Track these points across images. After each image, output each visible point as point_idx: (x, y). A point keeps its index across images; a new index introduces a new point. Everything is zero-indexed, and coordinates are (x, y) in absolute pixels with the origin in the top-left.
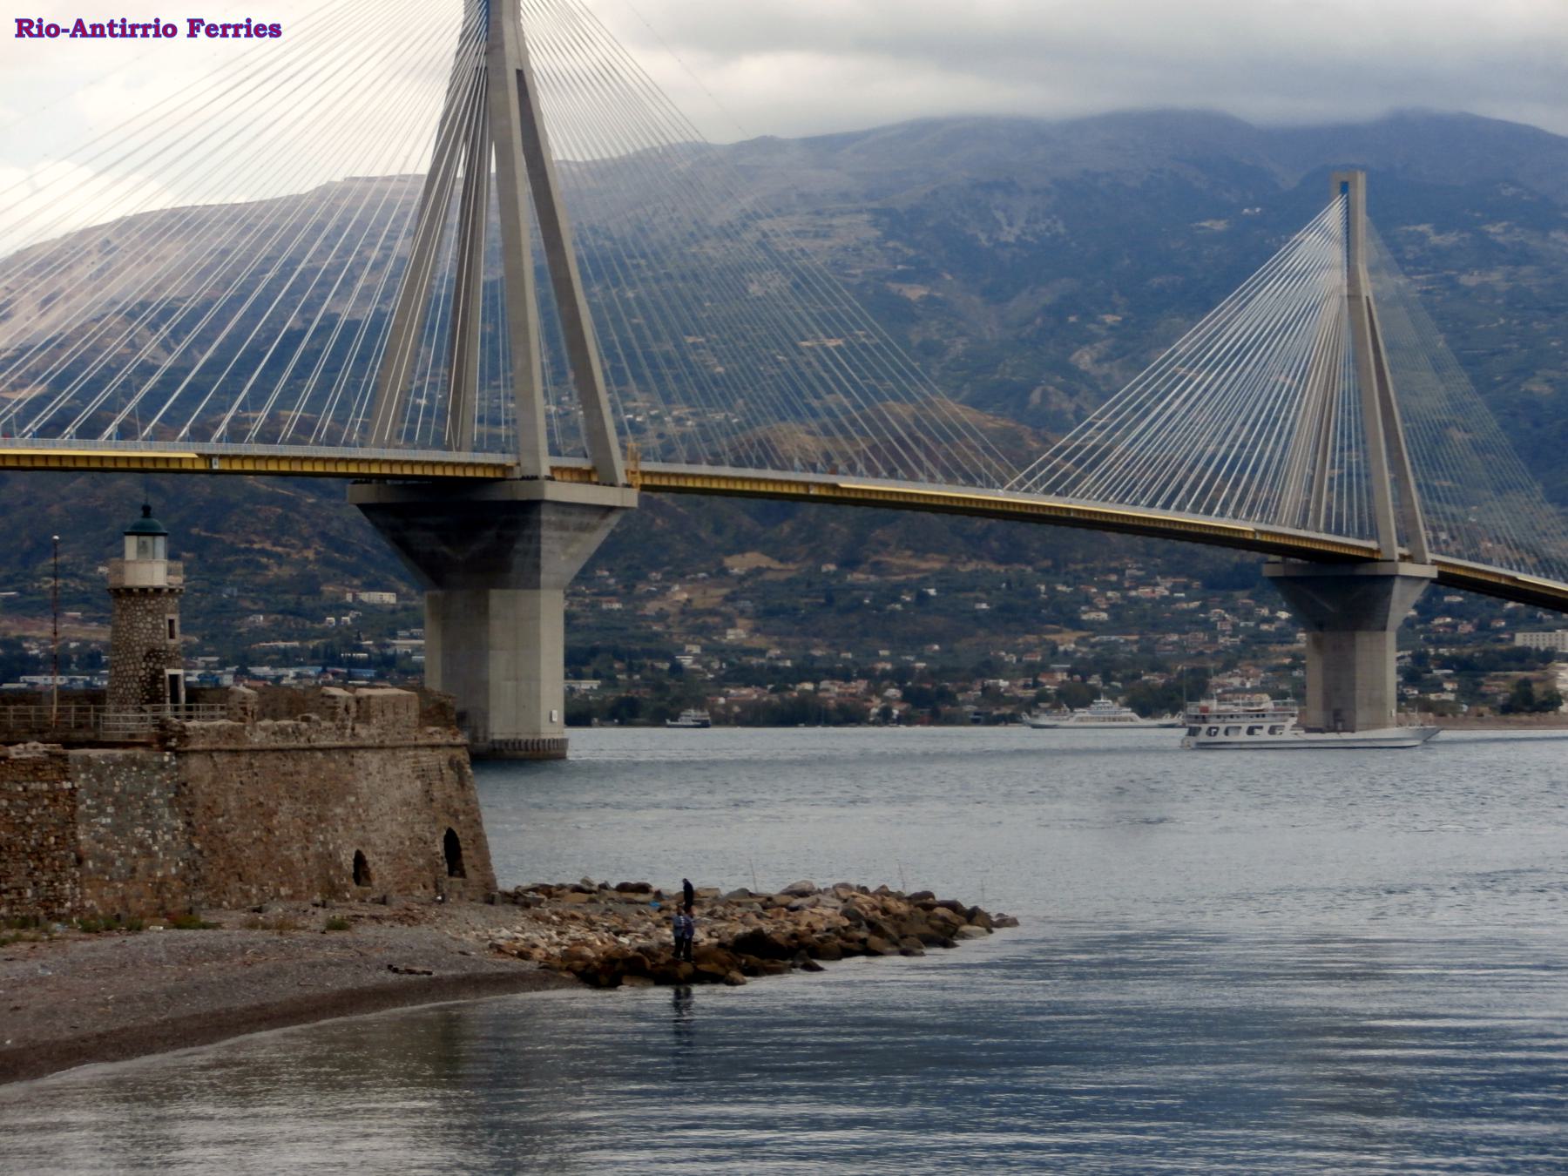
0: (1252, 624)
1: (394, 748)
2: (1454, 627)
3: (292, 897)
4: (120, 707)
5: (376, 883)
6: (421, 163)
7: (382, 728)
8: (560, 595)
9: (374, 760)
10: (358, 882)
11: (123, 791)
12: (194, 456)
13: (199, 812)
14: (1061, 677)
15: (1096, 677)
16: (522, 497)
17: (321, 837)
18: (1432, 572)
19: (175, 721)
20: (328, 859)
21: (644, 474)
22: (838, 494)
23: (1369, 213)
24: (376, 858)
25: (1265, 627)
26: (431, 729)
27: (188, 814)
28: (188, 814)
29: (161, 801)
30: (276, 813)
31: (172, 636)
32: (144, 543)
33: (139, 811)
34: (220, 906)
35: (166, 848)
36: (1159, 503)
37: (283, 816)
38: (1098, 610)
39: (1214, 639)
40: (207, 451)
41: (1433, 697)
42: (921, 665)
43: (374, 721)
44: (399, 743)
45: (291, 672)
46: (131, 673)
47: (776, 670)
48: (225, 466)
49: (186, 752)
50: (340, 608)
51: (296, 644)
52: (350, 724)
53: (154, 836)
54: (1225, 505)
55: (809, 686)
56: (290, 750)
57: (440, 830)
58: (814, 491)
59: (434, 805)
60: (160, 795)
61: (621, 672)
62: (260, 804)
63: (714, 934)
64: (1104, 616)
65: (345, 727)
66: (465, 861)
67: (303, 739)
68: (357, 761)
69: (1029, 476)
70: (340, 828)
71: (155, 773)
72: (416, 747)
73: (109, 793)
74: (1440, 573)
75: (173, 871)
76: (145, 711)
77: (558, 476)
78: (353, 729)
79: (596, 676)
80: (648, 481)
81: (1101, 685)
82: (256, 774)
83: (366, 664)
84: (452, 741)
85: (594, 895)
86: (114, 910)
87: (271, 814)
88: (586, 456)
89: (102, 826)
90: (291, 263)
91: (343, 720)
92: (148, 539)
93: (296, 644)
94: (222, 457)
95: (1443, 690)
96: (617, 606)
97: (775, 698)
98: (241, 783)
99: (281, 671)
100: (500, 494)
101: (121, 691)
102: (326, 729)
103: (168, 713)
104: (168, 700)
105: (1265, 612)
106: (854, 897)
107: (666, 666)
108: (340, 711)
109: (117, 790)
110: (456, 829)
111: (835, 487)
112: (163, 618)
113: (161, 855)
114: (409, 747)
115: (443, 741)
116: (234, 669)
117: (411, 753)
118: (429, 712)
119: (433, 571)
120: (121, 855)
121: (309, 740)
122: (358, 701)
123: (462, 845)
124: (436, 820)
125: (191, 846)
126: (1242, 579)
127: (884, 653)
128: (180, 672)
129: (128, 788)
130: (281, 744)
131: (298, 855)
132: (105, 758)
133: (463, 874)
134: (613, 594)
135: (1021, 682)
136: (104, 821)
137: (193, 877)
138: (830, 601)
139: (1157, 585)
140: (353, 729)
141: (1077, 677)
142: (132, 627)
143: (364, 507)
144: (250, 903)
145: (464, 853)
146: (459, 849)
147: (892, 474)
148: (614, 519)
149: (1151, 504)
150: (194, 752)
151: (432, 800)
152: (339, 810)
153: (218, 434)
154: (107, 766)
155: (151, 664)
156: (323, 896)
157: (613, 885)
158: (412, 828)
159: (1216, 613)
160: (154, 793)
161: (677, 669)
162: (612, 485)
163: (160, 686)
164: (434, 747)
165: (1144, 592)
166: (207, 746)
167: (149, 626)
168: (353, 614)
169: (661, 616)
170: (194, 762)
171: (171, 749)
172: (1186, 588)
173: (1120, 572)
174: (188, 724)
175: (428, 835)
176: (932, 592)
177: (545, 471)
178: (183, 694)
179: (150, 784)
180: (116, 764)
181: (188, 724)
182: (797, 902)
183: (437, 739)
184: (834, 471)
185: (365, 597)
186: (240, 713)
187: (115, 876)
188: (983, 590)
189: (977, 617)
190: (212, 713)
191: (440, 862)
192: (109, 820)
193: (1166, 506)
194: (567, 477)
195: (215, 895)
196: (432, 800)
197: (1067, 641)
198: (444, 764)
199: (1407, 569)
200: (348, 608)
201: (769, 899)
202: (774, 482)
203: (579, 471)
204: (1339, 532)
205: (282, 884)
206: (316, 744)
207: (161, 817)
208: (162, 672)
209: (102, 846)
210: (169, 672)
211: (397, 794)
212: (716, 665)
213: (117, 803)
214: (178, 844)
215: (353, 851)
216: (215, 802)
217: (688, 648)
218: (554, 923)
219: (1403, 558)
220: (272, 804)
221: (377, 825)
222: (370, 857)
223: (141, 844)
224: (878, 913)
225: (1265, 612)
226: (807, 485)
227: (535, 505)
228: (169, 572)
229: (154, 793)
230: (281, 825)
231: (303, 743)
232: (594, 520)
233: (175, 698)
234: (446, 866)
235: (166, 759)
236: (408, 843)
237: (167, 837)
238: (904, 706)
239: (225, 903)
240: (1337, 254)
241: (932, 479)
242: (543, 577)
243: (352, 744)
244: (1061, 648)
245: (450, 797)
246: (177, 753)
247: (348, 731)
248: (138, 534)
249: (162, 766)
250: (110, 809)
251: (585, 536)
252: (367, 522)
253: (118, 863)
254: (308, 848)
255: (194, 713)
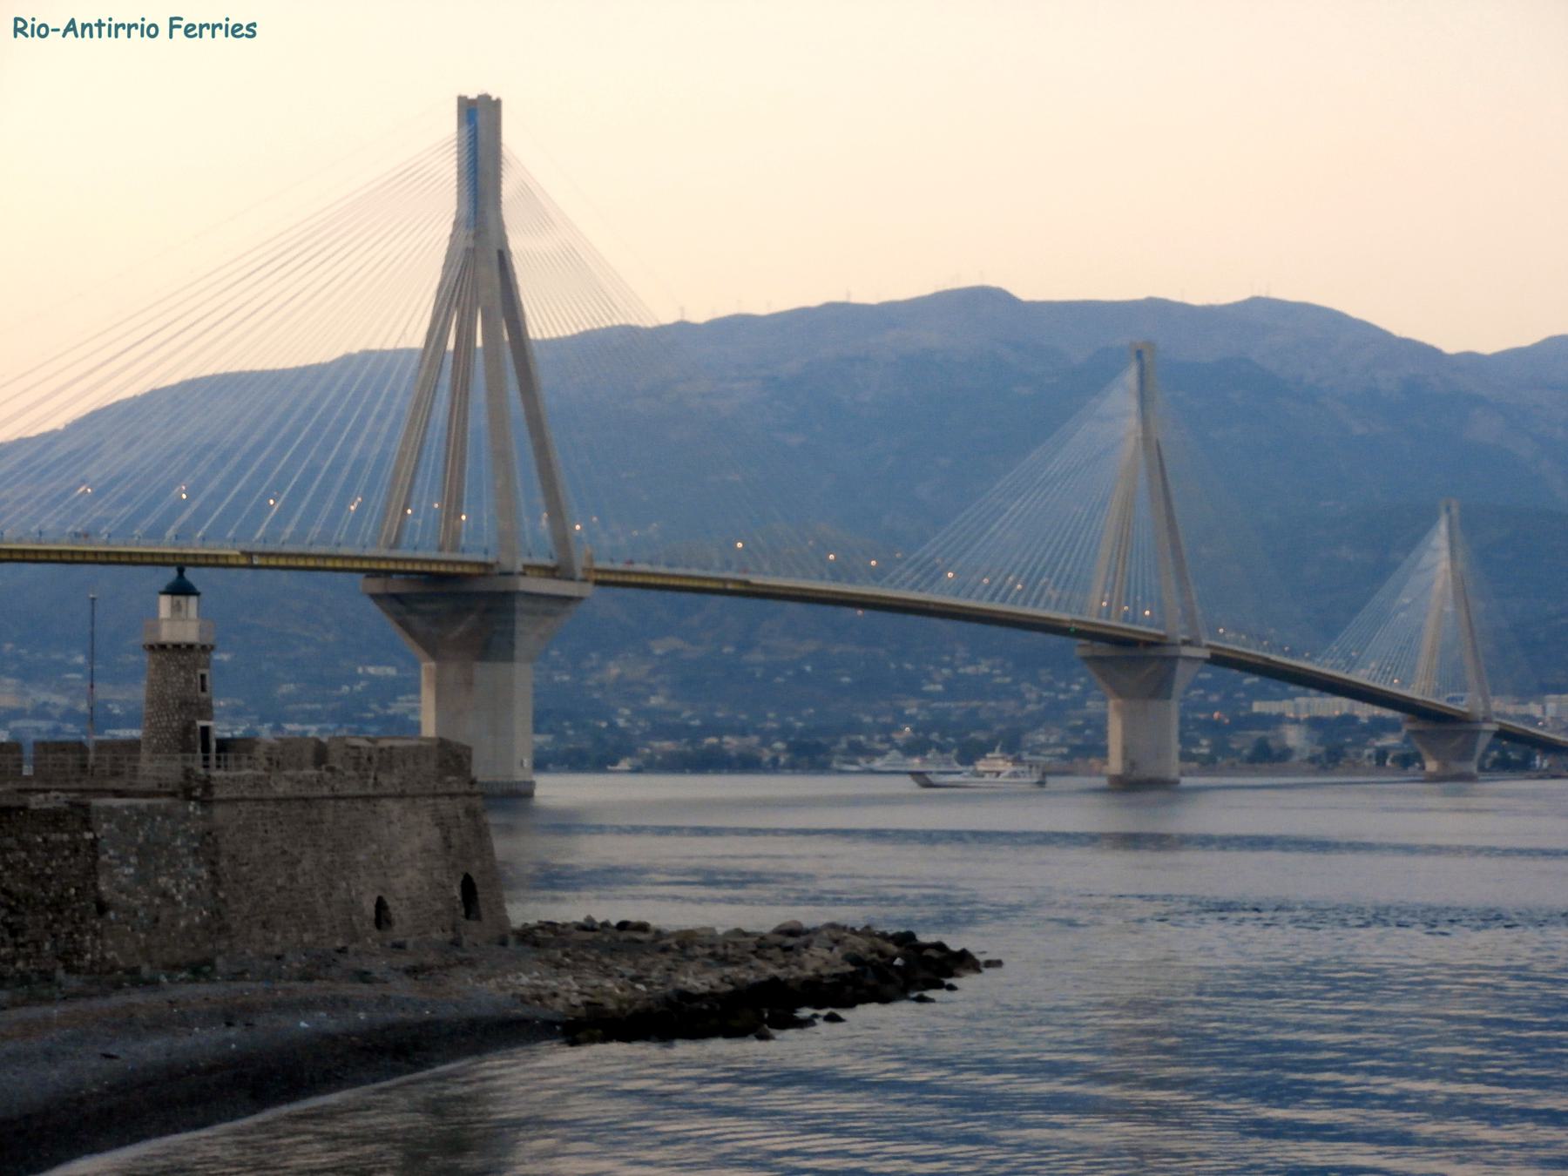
1: (414, 797)
2: (1205, 697)
6: (415, 338)
7: (404, 778)
9: (393, 807)
11: (147, 839)
12: (237, 553)
13: (224, 863)
16: (502, 588)
18: (1206, 654)
22: (749, 588)
24: (396, 904)
25: (1062, 697)
26: (450, 779)
27: (213, 863)
29: (185, 851)
30: (299, 861)
32: (178, 603)
33: (163, 861)
35: (190, 897)
36: (997, 599)
37: (307, 864)
38: (934, 682)
41: (1194, 751)
42: (800, 724)
43: (396, 771)
46: (164, 724)
47: (688, 728)
48: (263, 561)
50: (354, 679)
51: (319, 706)
52: (372, 774)
53: (178, 885)
55: (713, 740)
58: (730, 586)
59: (452, 850)
62: (284, 852)
63: (727, 980)
72: (435, 796)
77: (528, 572)
78: (375, 779)
79: (551, 731)
82: (281, 823)
87: (296, 862)
88: (551, 558)
90: (312, 410)
91: (366, 770)
92: (182, 599)
93: (319, 706)
94: (261, 555)
95: (1201, 746)
97: (689, 749)
98: (266, 831)
99: (307, 727)
100: (481, 586)
101: (155, 741)
102: (349, 778)
104: (199, 749)
106: (845, 938)
107: (604, 725)
108: (364, 761)
109: (140, 840)
110: (473, 874)
111: (747, 583)
112: (195, 673)
113: (185, 904)
114: (429, 796)
117: (430, 801)
121: (333, 789)
125: (215, 895)
127: (771, 715)
133: (478, 918)
135: (877, 737)
139: (979, 664)
140: (375, 779)
142: (166, 681)
143: (375, 597)
145: (480, 896)
149: (1025, 604)
150: (221, 801)
151: (450, 847)
155: (183, 717)
157: (614, 922)
159: (1025, 686)
160: (179, 842)
161: (612, 726)
163: (192, 736)
164: (452, 795)
165: (970, 670)
167: (183, 681)
168: (363, 684)
169: (601, 686)
171: (195, 799)
175: (446, 880)
176: (808, 668)
177: (519, 568)
178: (213, 745)
180: (140, 813)
182: (790, 941)
185: (371, 670)
191: (457, 906)
192: (132, 871)
193: (992, 598)
194: (536, 572)
196: (450, 847)
197: (911, 708)
198: (461, 812)
199: (1187, 651)
200: (357, 679)
201: (763, 938)
205: (306, 930)
206: (340, 793)
207: (185, 866)
208: (194, 722)
209: (124, 897)
210: (201, 723)
213: (142, 853)
215: (374, 898)
218: (568, 966)
219: (1185, 643)
220: (296, 852)
222: (390, 902)
223: (164, 894)
224: (875, 956)
225: (1063, 685)
226: (724, 581)
227: (508, 596)
229: (179, 842)
231: (326, 791)
233: (206, 748)
236: (427, 888)
237: (192, 887)
238: (788, 756)
240: (1133, 405)
245: (468, 844)
247: (371, 781)
249: (187, 817)
250: (133, 860)
253: (141, 914)
254: (331, 895)
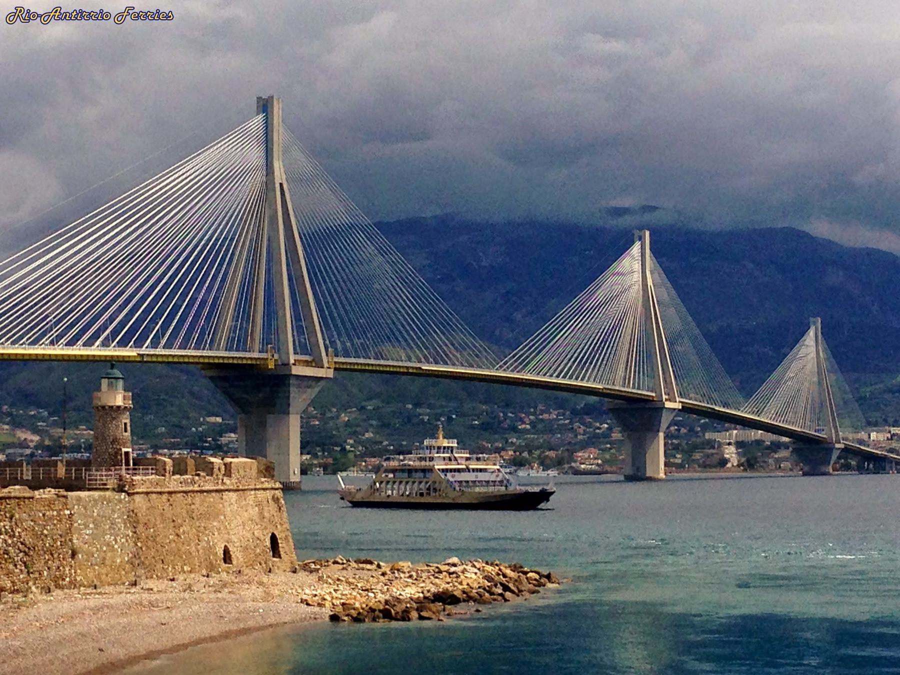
0: (591, 430)
3: (191, 572)
4: (98, 468)
5: (234, 562)
8: (299, 416)
9: (233, 496)
10: (225, 562)
14: (511, 453)
15: (526, 453)
17: (206, 539)
19: (128, 476)
20: (210, 549)
21: (335, 363)
22: (421, 372)
23: (651, 250)
25: (598, 431)
26: (263, 480)
28: (135, 527)
31: (126, 431)
33: (108, 526)
34: (152, 577)
38: (524, 423)
39: (576, 436)
40: (141, 353)
44: (246, 487)
45: (177, 452)
48: (149, 359)
49: (134, 494)
51: (179, 440)
53: (116, 540)
54: (589, 378)
56: (189, 492)
57: (267, 534)
58: (411, 371)
59: (265, 520)
60: (119, 517)
61: (319, 451)
64: (528, 427)
65: (218, 479)
66: (281, 549)
67: (196, 486)
68: (224, 497)
69: (505, 364)
70: (216, 533)
71: (116, 505)
72: (255, 489)
73: (92, 517)
74: (682, 407)
75: (126, 559)
76: (111, 471)
78: (223, 480)
80: (337, 366)
81: (528, 456)
83: (208, 449)
84: (273, 486)
85: (345, 566)
86: (93, 581)
89: (87, 535)
93: (179, 440)
96: (317, 423)
99: (172, 451)
103: (123, 472)
105: (598, 424)
106: (484, 567)
110: (275, 533)
111: (420, 368)
114: (252, 490)
115: (270, 486)
116: (152, 450)
118: (261, 471)
119: (243, 406)
120: (97, 551)
122: (225, 464)
123: (279, 541)
124: (266, 528)
126: (589, 410)
128: (130, 450)
129: (102, 513)
130: (184, 489)
131: (194, 548)
132: (89, 497)
133: (280, 557)
134: (316, 418)
136: (88, 532)
137: (137, 561)
138: (409, 421)
141: (518, 453)
144: (168, 575)
146: (278, 543)
147: (437, 363)
148: (322, 383)
150: (137, 493)
152: (215, 524)
153: (146, 345)
154: (90, 501)
156: (207, 570)
158: (253, 533)
160: (116, 516)
162: (322, 367)
166: (145, 490)
168: (204, 427)
170: (137, 498)
172: (564, 415)
173: (535, 408)
174: (134, 478)
176: (454, 416)
177: (292, 361)
179: (113, 511)
181: (134, 478)
183: (266, 485)
184: (420, 362)
186: (163, 472)
187: (94, 562)
188: (475, 415)
189: (473, 427)
190: (147, 472)
193: (558, 376)
195: (149, 571)
198: (270, 498)
199: (668, 405)
200: (201, 424)
202: (393, 366)
203: (306, 361)
204: (639, 388)
205: (185, 565)
210: (124, 450)
211: (246, 514)
212: (360, 448)
214: (129, 545)
215: (223, 547)
216: (149, 520)
217: (348, 441)
221: (236, 531)
223: (108, 545)
226: (407, 368)
228: (124, 398)
229: (116, 516)
230: (184, 532)
231: (196, 488)
232: (313, 384)
233: (127, 464)
234: (271, 553)
235: (122, 497)
239: (154, 576)
240: (637, 266)
241: (454, 364)
242: (291, 409)
243: (222, 488)
244: (510, 441)
246: (129, 494)
248: (109, 378)
249: (120, 501)
250: (91, 526)
251: (309, 390)
252: (212, 385)
255: (137, 472)
